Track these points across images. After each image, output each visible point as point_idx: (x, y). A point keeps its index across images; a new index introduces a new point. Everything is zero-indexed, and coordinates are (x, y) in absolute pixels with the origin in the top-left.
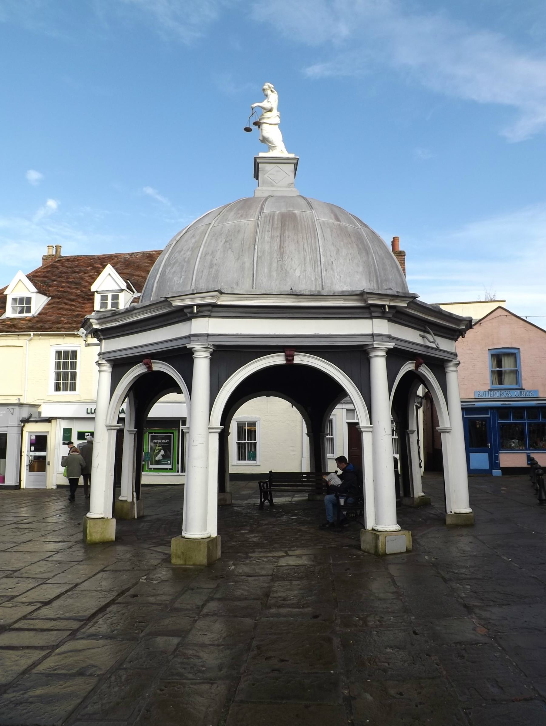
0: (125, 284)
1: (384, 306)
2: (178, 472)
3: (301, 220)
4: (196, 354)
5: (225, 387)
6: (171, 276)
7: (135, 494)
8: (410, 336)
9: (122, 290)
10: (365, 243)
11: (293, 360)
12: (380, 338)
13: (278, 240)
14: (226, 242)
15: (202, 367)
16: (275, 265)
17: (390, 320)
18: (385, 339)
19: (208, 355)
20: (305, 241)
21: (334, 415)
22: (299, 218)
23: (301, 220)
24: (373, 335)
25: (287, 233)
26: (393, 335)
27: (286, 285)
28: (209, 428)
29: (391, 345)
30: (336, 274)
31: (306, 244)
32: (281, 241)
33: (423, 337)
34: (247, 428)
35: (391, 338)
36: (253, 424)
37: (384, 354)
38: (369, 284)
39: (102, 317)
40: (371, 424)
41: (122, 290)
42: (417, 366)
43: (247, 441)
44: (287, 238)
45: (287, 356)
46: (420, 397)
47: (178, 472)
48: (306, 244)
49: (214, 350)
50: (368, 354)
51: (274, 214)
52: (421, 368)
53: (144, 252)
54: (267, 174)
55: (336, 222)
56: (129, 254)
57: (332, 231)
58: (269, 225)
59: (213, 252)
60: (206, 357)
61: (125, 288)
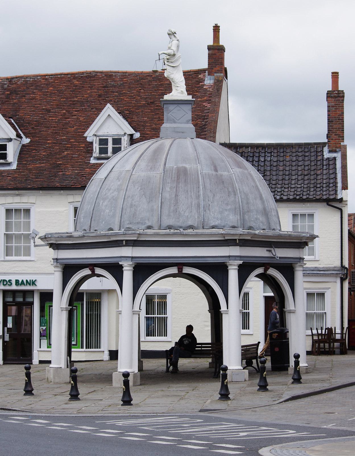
0: (15, 133)
1: (236, 240)
2: (82, 347)
3: (190, 174)
4: (124, 269)
5: (142, 287)
6: (103, 208)
7: (68, 358)
8: (259, 253)
9: (10, 140)
10: (234, 186)
11: (182, 271)
12: (234, 258)
13: (175, 190)
14: (141, 189)
15: (128, 276)
16: (172, 208)
17: (240, 246)
18: (237, 258)
19: (132, 269)
20: (192, 191)
21: (251, 288)
22: (189, 172)
23: (190, 174)
24: (229, 257)
25: (180, 185)
26: (242, 255)
27: (179, 222)
28: (133, 311)
29: (241, 262)
30: (211, 214)
31: (192, 193)
32: (176, 191)
33: (270, 251)
34: (156, 300)
35: (240, 257)
36: (164, 297)
37: (237, 267)
38: (234, 217)
39: (60, 237)
40: (228, 309)
41: (10, 140)
42: (266, 270)
43: (156, 316)
44: (180, 189)
45: (178, 269)
46: (346, 268)
47: (82, 347)
48: (192, 193)
49: (135, 265)
50: (227, 267)
51: (173, 168)
52: (269, 270)
53: (27, 77)
54: (170, 113)
55: (214, 173)
56: (7, 79)
57: (210, 180)
58: (169, 178)
59: (132, 196)
60: (130, 270)
61: (15, 137)
